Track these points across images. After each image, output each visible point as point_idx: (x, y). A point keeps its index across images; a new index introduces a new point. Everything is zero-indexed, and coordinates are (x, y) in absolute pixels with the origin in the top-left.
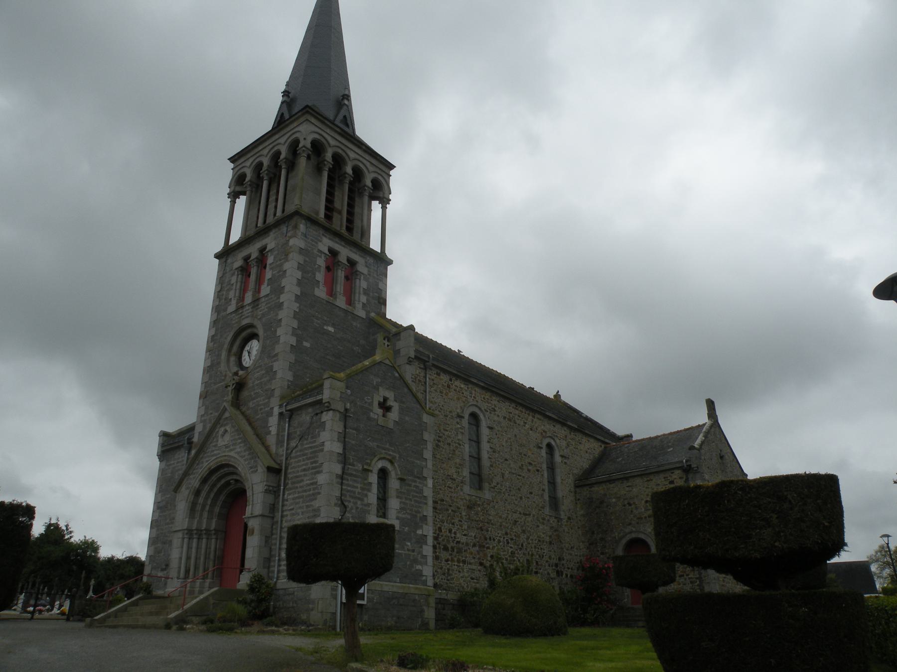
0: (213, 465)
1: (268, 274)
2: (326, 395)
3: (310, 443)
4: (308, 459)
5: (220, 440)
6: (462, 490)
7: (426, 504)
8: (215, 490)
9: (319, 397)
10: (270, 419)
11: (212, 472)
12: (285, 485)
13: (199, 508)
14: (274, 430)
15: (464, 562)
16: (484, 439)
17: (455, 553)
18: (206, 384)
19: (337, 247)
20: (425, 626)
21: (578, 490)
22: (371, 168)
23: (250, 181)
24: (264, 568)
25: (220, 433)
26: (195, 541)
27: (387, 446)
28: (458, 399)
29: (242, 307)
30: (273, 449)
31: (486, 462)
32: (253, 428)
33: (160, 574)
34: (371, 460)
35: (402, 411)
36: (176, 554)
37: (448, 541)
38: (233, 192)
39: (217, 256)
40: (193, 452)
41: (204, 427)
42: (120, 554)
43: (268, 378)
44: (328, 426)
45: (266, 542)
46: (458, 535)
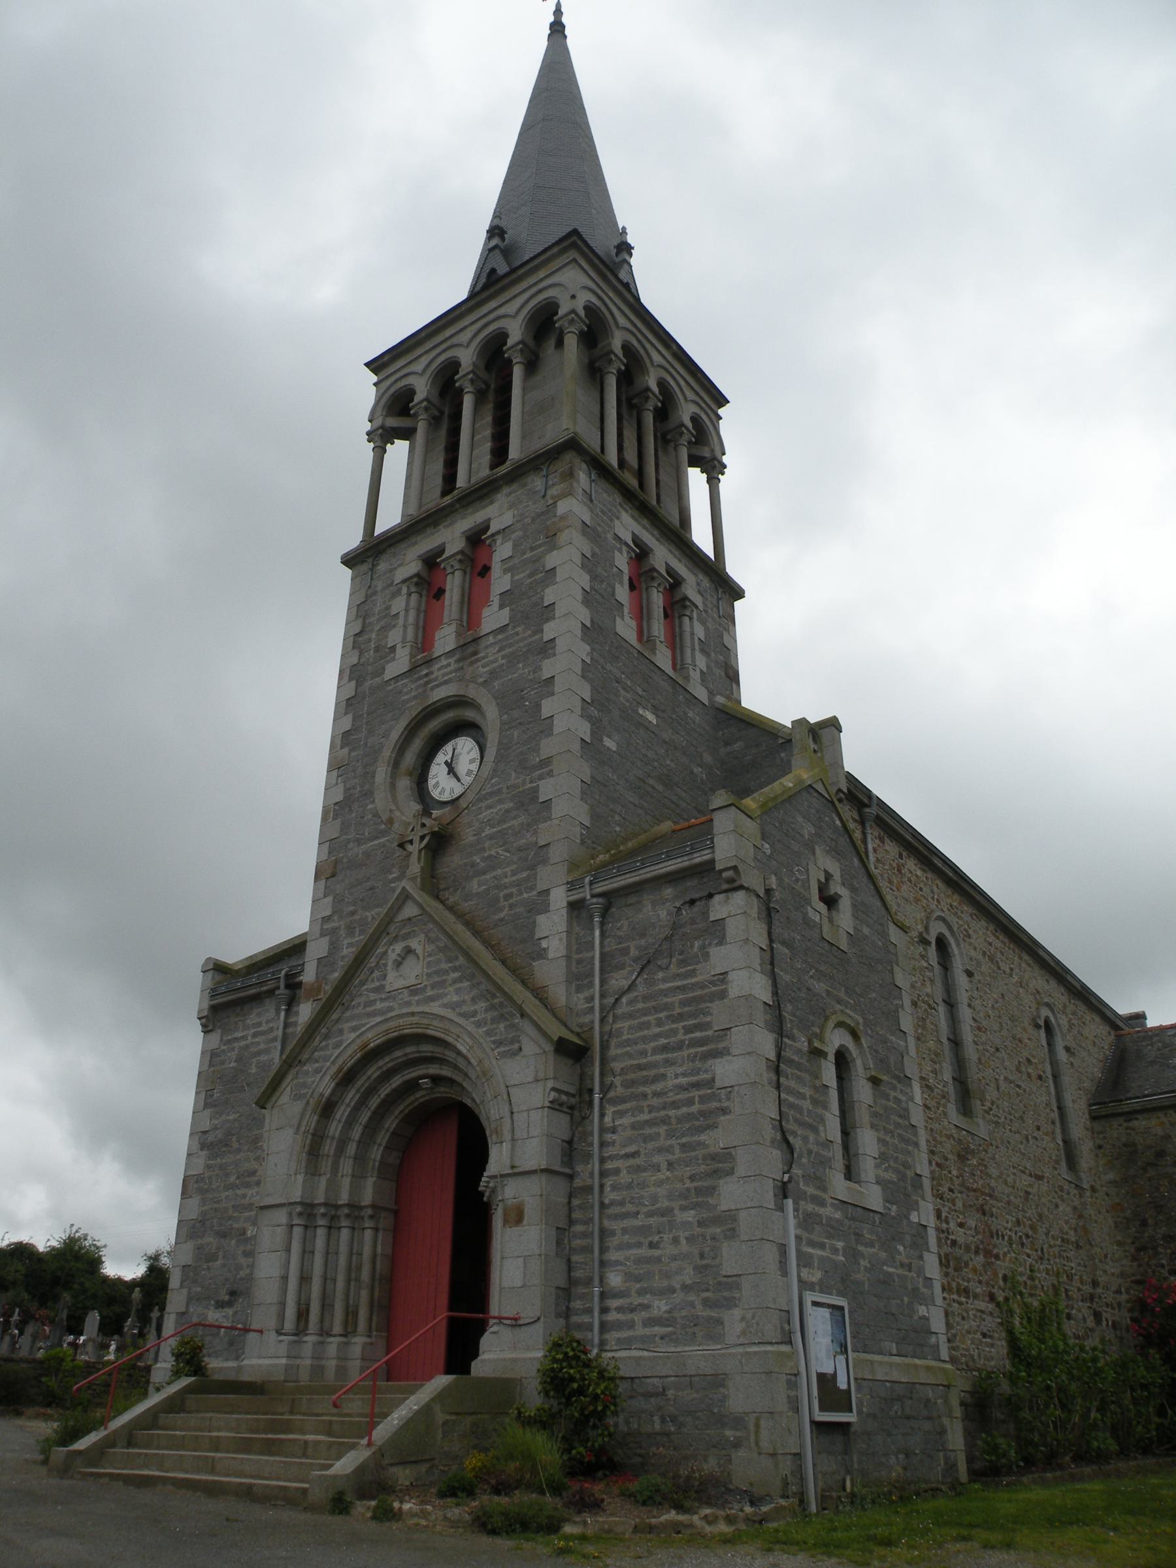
0: (374, 1038)
1: (500, 582)
3: (677, 976)
5: (391, 975)
7: (916, 1145)
8: (374, 1102)
9: (698, 858)
10: (541, 919)
11: (370, 1056)
12: (605, 1089)
13: (329, 1148)
16: (962, 997)
17: (951, 1270)
18: (329, 843)
19: (649, 539)
22: (690, 395)
23: (426, 399)
24: (558, 1315)
26: (321, 1233)
27: (842, 995)
28: (917, 900)
29: (429, 662)
30: (559, 994)
31: (971, 1052)
32: (487, 943)
33: (214, 1316)
34: (822, 1027)
35: (859, 910)
36: (272, 1265)
38: (382, 427)
39: (349, 560)
40: (305, 1011)
41: (334, 947)
43: (523, 819)
44: (733, 929)
45: (559, 1243)
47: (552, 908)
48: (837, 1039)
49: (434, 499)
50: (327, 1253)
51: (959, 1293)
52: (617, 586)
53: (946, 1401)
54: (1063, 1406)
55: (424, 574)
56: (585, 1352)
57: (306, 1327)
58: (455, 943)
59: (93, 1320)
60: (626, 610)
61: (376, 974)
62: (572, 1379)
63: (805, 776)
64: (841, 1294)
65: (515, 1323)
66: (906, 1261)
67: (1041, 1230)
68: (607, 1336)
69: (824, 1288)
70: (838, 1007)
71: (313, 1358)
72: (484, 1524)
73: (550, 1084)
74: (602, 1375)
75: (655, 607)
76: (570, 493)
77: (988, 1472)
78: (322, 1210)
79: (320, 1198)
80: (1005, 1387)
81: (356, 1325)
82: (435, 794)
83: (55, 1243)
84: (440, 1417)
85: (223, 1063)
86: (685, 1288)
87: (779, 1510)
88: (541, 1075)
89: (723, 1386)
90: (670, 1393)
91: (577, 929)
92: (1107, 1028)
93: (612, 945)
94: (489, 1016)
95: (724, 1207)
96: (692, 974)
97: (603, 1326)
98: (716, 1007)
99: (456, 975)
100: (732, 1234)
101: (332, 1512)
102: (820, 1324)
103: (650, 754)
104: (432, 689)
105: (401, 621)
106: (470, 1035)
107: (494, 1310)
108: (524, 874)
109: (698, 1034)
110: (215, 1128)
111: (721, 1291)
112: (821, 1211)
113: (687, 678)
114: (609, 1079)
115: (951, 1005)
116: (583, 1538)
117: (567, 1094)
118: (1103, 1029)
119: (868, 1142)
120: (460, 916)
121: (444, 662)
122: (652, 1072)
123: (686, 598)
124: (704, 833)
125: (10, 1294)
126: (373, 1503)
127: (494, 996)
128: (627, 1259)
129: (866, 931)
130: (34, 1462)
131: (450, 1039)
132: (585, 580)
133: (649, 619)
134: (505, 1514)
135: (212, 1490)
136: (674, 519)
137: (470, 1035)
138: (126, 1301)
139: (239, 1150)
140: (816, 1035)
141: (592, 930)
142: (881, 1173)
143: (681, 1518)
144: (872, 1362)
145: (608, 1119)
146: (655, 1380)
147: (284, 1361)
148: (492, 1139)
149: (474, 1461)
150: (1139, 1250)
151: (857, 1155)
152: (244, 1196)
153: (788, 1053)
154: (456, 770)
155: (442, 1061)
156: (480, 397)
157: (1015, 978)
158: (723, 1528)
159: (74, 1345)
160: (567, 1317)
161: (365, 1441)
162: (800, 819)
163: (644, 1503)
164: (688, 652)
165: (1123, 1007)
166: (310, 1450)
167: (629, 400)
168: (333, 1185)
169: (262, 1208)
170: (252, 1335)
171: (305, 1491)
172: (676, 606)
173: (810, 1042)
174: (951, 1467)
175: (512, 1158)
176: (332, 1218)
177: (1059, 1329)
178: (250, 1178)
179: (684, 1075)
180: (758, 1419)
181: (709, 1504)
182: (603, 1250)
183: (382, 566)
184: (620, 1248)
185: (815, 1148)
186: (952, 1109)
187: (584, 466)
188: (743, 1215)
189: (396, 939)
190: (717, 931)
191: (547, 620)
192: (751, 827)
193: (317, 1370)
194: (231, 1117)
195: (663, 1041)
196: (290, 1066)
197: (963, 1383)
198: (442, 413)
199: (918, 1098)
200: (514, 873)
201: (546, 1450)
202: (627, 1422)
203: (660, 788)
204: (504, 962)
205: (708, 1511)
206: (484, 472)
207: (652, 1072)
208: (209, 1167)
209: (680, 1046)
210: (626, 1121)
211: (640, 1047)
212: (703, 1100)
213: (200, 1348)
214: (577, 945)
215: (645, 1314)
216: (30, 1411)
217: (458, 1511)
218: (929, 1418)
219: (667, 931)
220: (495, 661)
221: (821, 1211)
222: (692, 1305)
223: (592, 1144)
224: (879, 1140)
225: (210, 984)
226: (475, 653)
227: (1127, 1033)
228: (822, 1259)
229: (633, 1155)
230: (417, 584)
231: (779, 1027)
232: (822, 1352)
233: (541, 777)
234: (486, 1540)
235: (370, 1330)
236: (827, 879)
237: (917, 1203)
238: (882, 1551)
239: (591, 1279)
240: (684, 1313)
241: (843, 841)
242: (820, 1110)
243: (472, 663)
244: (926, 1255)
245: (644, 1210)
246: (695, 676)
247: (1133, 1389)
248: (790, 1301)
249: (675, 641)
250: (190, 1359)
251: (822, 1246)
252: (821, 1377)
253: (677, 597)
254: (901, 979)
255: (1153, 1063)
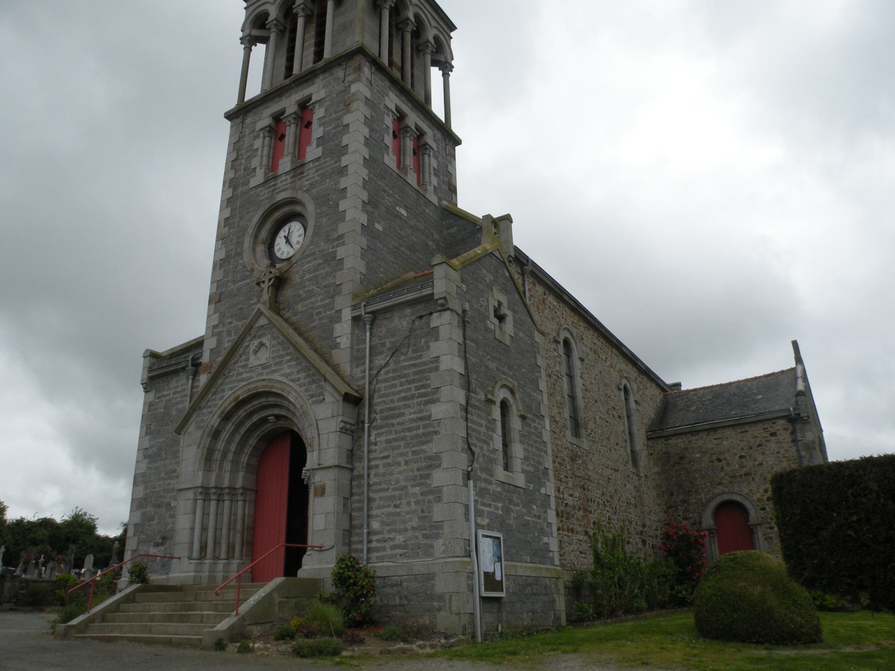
0: (242, 394)
1: (317, 131)
2: (440, 288)
4: (410, 382)
5: (252, 358)
7: (546, 452)
8: (243, 430)
9: (425, 292)
10: (337, 327)
11: (240, 404)
12: (371, 421)
13: (217, 456)
14: (344, 342)
16: (577, 372)
17: (564, 519)
19: (405, 108)
21: (650, 443)
22: (433, 23)
23: (276, 19)
25: (252, 347)
26: (213, 503)
27: (506, 370)
28: (553, 319)
29: (275, 177)
30: (346, 368)
31: (581, 403)
32: (306, 340)
33: (153, 551)
34: (494, 388)
35: (517, 323)
36: (185, 521)
38: (249, 35)
39: (229, 116)
40: (203, 379)
41: (220, 342)
42: (31, 516)
43: (328, 269)
44: (443, 332)
45: (345, 506)
47: (343, 320)
48: (501, 394)
49: (280, 80)
50: (217, 514)
51: (568, 530)
52: (386, 135)
53: (556, 586)
54: (620, 587)
55: (273, 126)
56: (358, 564)
57: (205, 555)
58: (288, 339)
59: (90, 559)
60: (390, 150)
61: (243, 357)
62: (350, 578)
63: (488, 247)
64: (499, 531)
65: (321, 549)
66: (537, 514)
67: (616, 498)
68: (371, 555)
69: (490, 527)
70: (503, 376)
71: (209, 572)
72: (299, 653)
73: (340, 419)
74: (366, 575)
75: (408, 149)
76: (358, 80)
77: (577, 620)
78: (214, 491)
79: (212, 484)
80: (590, 579)
81: (234, 553)
82: (278, 254)
83: (66, 518)
84: (277, 599)
85: (156, 409)
86: (413, 528)
87: (460, 642)
88: (335, 414)
89: (432, 579)
90: (405, 584)
91: (356, 332)
92: (659, 391)
93: (376, 341)
94: (307, 381)
95: (435, 485)
96: (420, 357)
97: (369, 550)
98: (433, 375)
99: (288, 358)
100: (439, 499)
101: (216, 650)
102: (487, 548)
103: (403, 233)
104: (277, 193)
105: (259, 153)
106: (296, 391)
107: (310, 543)
108: (328, 301)
109: (422, 391)
110: (152, 446)
111: (432, 529)
112: (490, 487)
113: (426, 190)
114: (373, 416)
115: (571, 377)
116: (352, 657)
117: (350, 424)
118: (657, 391)
119: (518, 450)
120: (291, 324)
121: (284, 178)
122: (397, 412)
123: (426, 144)
124: (428, 279)
125: (39, 547)
126: (238, 644)
127: (309, 370)
128: (382, 514)
129: (521, 334)
130: (47, 633)
131: (284, 394)
132: (366, 131)
133: (404, 155)
134: (310, 647)
135: (149, 642)
136: (422, 98)
137: (296, 391)
138: (110, 549)
139: (166, 459)
140: (489, 391)
141: (365, 332)
142: (525, 468)
143: (406, 646)
144: (515, 566)
145: (372, 438)
146: (396, 578)
147: (193, 574)
148: (308, 449)
149: (295, 622)
150: (668, 508)
151: (511, 457)
152: (169, 484)
153: (473, 402)
154: (291, 241)
155: (280, 406)
156: (308, 20)
157: (608, 363)
158: (429, 650)
159: (79, 574)
160: (349, 545)
161: (235, 613)
162: (485, 272)
163: (387, 640)
164: (427, 175)
165: (669, 380)
166: (205, 619)
167: (397, 25)
168: (219, 477)
169: (179, 490)
170: (174, 561)
171: (200, 640)
172: (421, 148)
173: (486, 395)
174: (557, 618)
175: (319, 459)
176: (220, 495)
177: (623, 548)
178: (173, 474)
179: (415, 413)
180: (451, 596)
181: (422, 639)
182: (368, 510)
183: (249, 120)
184: (378, 508)
185: (487, 453)
186: (568, 434)
187: (368, 64)
188: (445, 489)
189: (254, 337)
190: (434, 333)
191: (344, 155)
192: (455, 275)
193: (212, 579)
194: (162, 440)
195: (403, 394)
196: (195, 410)
197: (567, 577)
198: (285, 28)
199: (548, 427)
200: (322, 300)
201: (334, 615)
202: (381, 600)
203: (408, 253)
204: (316, 351)
205: (421, 642)
206: (309, 65)
207: (397, 412)
208: (149, 468)
209: (413, 397)
210: (382, 438)
211: (391, 398)
212: (425, 426)
213: (145, 569)
214: (357, 341)
215: (391, 543)
216: (49, 609)
217: (284, 647)
218: (546, 594)
219: (407, 333)
220: (313, 178)
221: (490, 487)
222: (417, 537)
223: (363, 452)
224: (524, 449)
225: (148, 364)
226: (302, 173)
227: (671, 395)
228: (489, 513)
229: (386, 457)
230: (269, 132)
231: (468, 387)
232: (487, 557)
233: (338, 246)
234: (299, 660)
235: (242, 556)
236: (499, 306)
237: (545, 483)
238: (510, 657)
239: (362, 525)
240: (412, 542)
241: (510, 285)
242: (491, 433)
243: (300, 179)
244: (549, 511)
245: (392, 487)
246: (431, 189)
247: (658, 577)
248: (470, 535)
249: (419, 169)
250: (139, 574)
251: (489, 506)
252: (486, 574)
253: (422, 143)
254: (540, 362)
255: (681, 410)
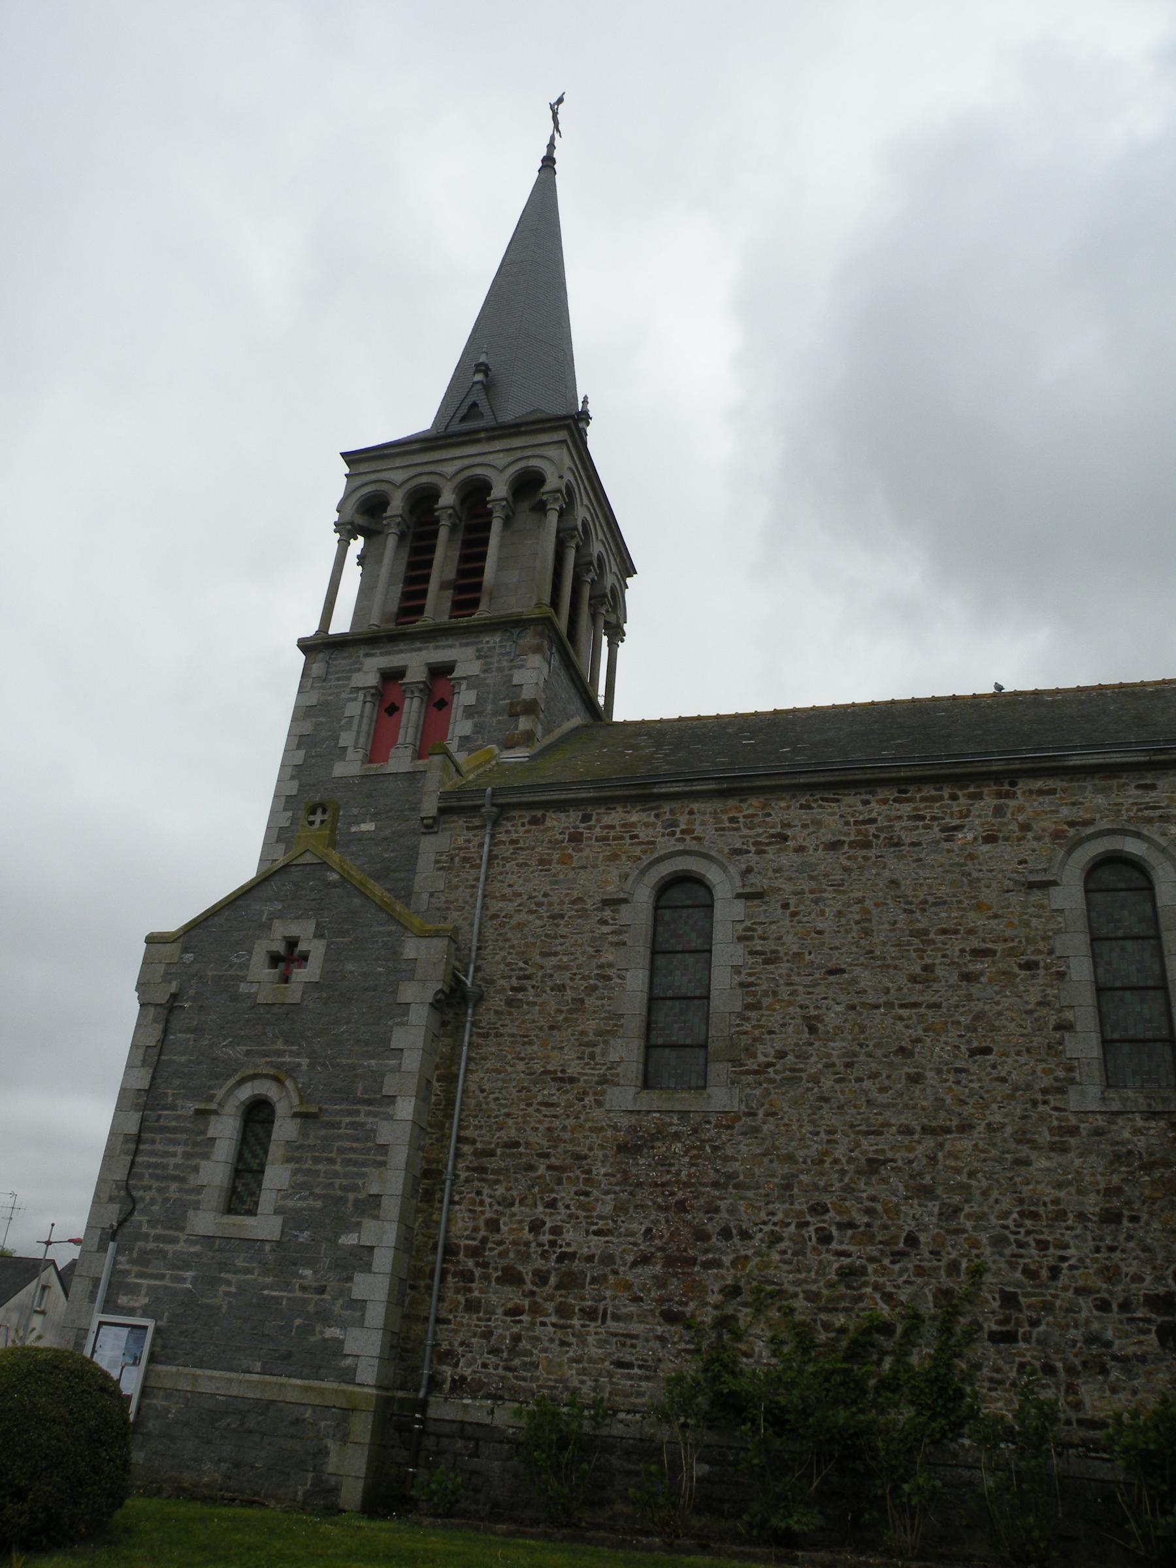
6: (600, 1104)
15: (590, 1314)
20: (325, 1501)
27: (279, 1045)
37: (525, 1257)
42: (364, 1467)
46: (569, 1236)
